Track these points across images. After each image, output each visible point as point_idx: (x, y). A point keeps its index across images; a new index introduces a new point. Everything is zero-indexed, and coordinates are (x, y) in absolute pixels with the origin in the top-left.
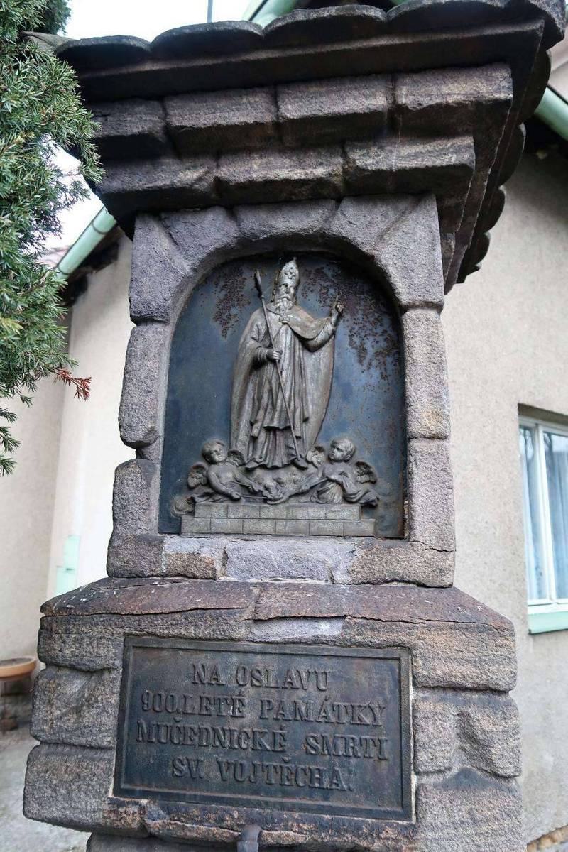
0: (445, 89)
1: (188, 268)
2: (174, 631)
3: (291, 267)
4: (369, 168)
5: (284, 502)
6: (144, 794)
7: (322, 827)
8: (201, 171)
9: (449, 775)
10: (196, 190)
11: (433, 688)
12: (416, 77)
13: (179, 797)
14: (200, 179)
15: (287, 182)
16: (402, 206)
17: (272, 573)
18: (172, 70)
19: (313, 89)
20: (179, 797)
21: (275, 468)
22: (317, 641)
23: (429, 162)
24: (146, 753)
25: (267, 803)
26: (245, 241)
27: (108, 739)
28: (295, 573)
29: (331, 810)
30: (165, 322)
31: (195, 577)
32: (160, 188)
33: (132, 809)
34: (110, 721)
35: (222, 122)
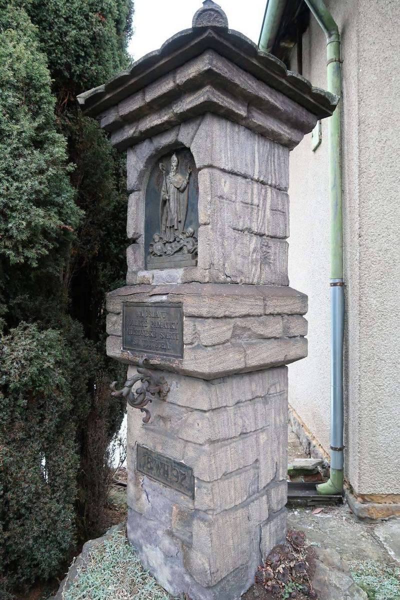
0: (189, 72)
1: (142, 167)
2: (131, 300)
3: (174, 158)
4: (178, 112)
5: (172, 255)
6: (129, 349)
7: (162, 360)
8: (134, 129)
9: (194, 345)
10: (135, 136)
11: (189, 317)
12: (182, 69)
13: (135, 350)
14: (134, 132)
15: (157, 126)
16: (198, 122)
17: (164, 281)
18: (113, 96)
19: (192, 63)
20: (135, 350)
21: (171, 242)
22: (162, 302)
23: (198, 102)
24: (129, 338)
25: (156, 353)
26: (157, 151)
27: (120, 334)
28: (169, 281)
29: (167, 355)
30: (139, 190)
31: (145, 284)
32: (125, 139)
33: (125, 353)
34: (120, 328)
35: (131, 110)
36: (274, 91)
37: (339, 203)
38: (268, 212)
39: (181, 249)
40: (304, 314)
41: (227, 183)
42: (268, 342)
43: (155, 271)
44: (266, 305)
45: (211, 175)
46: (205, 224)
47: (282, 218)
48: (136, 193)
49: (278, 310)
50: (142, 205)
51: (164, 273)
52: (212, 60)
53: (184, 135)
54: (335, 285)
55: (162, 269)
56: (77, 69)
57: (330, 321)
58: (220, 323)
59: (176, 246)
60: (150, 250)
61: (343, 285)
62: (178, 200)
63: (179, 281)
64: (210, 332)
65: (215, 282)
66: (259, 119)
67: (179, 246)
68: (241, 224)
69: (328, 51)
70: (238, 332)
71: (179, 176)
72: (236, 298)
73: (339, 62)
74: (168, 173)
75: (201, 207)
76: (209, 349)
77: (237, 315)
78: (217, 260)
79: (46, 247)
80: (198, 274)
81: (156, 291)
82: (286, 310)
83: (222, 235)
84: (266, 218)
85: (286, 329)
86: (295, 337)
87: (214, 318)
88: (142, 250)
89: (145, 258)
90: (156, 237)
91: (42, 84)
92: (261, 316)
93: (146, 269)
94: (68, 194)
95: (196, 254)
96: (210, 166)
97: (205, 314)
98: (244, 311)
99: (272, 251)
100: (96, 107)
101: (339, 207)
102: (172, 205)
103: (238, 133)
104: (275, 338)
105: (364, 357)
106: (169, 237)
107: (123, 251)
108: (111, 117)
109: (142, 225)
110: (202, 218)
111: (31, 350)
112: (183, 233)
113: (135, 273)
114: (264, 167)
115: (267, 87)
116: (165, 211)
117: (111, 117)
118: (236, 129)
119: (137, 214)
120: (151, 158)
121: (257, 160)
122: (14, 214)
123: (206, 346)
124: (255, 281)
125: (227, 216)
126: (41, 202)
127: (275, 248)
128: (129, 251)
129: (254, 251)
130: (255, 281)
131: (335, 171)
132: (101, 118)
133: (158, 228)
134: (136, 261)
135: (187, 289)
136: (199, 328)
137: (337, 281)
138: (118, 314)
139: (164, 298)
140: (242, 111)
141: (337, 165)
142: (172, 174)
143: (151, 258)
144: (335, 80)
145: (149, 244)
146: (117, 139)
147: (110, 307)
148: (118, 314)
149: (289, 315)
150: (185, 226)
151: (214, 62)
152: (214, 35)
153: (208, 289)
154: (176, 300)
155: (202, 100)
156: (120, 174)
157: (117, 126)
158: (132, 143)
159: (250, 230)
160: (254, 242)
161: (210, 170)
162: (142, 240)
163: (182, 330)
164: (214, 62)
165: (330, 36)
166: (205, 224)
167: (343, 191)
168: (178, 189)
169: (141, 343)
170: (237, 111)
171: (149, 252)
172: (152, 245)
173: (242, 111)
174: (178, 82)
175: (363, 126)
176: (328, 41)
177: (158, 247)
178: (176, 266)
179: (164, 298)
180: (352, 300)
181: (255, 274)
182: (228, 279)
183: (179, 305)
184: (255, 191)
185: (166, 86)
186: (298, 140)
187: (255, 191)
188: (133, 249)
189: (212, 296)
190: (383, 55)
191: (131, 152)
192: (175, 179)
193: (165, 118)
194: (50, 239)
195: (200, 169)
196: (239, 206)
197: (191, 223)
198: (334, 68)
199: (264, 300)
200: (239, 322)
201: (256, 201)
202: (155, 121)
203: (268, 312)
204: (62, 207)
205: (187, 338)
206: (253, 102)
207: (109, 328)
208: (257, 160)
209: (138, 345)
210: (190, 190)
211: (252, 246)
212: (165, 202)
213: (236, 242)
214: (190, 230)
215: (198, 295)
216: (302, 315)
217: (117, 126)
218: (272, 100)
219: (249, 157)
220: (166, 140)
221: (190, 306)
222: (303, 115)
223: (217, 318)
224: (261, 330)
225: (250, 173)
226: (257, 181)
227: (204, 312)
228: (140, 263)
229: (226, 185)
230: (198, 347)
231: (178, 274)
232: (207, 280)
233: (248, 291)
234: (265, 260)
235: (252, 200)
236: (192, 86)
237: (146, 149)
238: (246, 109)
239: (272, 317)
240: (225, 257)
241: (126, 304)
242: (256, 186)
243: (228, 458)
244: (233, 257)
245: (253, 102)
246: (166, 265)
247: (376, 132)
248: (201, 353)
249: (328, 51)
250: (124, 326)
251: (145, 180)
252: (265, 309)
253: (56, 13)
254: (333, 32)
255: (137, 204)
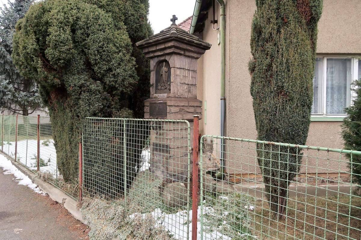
3: (164, 63)
27: (149, 112)
30: (154, 71)
36: (191, 46)
37: (224, 69)
38: (190, 78)
39: (166, 88)
40: (201, 107)
41: (179, 71)
42: (190, 113)
43: (159, 94)
44: (189, 103)
45: (174, 70)
46: (173, 82)
47: (195, 79)
48: (153, 72)
49: (192, 105)
50: (155, 75)
51: (161, 95)
52: (174, 43)
53: (167, 58)
54: (222, 99)
55: (161, 93)
56: (135, 35)
57: (220, 113)
58: (176, 107)
59: (165, 87)
60: (157, 88)
61: (225, 99)
62: (165, 75)
63: (166, 97)
64: (173, 109)
65: (175, 97)
66: (187, 54)
67: (166, 87)
68: (182, 82)
69: (221, 11)
70: (181, 110)
71: (166, 68)
72: (181, 101)
73: (224, 15)
74: (162, 67)
75: (171, 78)
76: (173, 113)
77: (181, 105)
78: (176, 91)
79: (131, 88)
80: (171, 95)
81: (159, 99)
82: (195, 105)
83: (177, 85)
84: (190, 80)
85: (195, 110)
86: (198, 113)
87: (175, 106)
88: (155, 88)
89: (156, 90)
90: (159, 85)
91: (100, 5)
92: (188, 106)
93: (156, 93)
94: (135, 75)
95: (170, 90)
96: (174, 67)
97: (172, 105)
98: (183, 104)
99: (191, 89)
100: (142, 47)
101: (223, 70)
102: (164, 76)
103: (182, 58)
104: (192, 113)
105: (230, 125)
106: (163, 84)
107: (149, 88)
108: (146, 50)
109: (155, 81)
110: (172, 81)
111: (127, 115)
112: (167, 84)
113: (153, 95)
114: (189, 66)
115: (189, 46)
116: (162, 77)
117: (146, 50)
118: (181, 56)
119: (153, 77)
120: (157, 63)
121: (187, 64)
122: (126, 80)
123: (173, 113)
124: (186, 97)
125: (178, 80)
126: (131, 76)
127: (192, 88)
128: (151, 89)
129: (186, 89)
130: (186, 97)
131: (222, 57)
132: (143, 50)
133: (159, 82)
134: (153, 91)
135: (168, 99)
136: (171, 108)
137: (223, 98)
138: (148, 106)
139: (162, 101)
140: (182, 53)
141: (223, 55)
142: (163, 67)
143: (157, 90)
144: (223, 22)
145: (157, 86)
146: (147, 56)
147: (146, 104)
148: (148, 106)
149: (196, 107)
150: (167, 82)
151: (175, 43)
152: (175, 38)
153: (173, 99)
154: (165, 102)
155: (172, 51)
156: (148, 66)
157: (149, 53)
158: (152, 58)
159: (185, 83)
160: (186, 87)
161: (174, 68)
162: (155, 85)
163: (167, 109)
164: (175, 43)
165: (221, 5)
166: (173, 82)
167: (225, 64)
168: (165, 72)
169: (155, 114)
170: (181, 53)
171: (157, 89)
172: (158, 87)
173: (182, 53)
174: (166, 46)
175: (230, 42)
176: (221, 7)
177: (160, 87)
178: (165, 93)
179: (162, 101)
180: (227, 104)
181: (186, 95)
182: (179, 96)
183: (166, 103)
184: (187, 73)
185: (163, 46)
186: (200, 57)
187: (187, 73)
188: (152, 88)
189: (175, 100)
190: (238, 16)
191: (152, 60)
192: (164, 69)
193: (162, 53)
194: (132, 86)
195: (171, 68)
196: (182, 77)
197: (169, 81)
198: (222, 17)
199: (188, 102)
200: (182, 108)
201: (187, 75)
202: (159, 53)
203: (189, 105)
204: (134, 77)
205: (168, 111)
206: (185, 50)
207: (145, 110)
208: (187, 64)
209: (154, 115)
210: (169, 73)
211: (185, 88)
212: (162, 75)
213: (181, 86)
214: (169, 83)
215: (171, 100)
216: (200, 107)
217: (149, 53)
218: (190, 49)
219: (185, 64)
220: (162, 58)
221: (169, 103)
222: (200, 50)
223: (176, 106)
224: (187, 110)
225: (185, 68)
226: (187, 70)
227: (172, 104)
228: (154, 91)
229: (178, 72)
230: (171, 113)
231: (166, 95)
232: (173, 96)
233: (184, 100)
234: (189, 91)
235: (186, 75)
236: (170, 47)
237: (156, 60)
238: (183, 52)
239: (191, 107)
240: (178, 91)
241: (151, 103)
242: (187, 71)
243: (178, 143)
244: (180, 90)
245: (185, 50)
246: (162, 92)
247: (235, 44)
248: (171, 115)
249: (221, 11)
250: (150, 109)
251: (156, 68)
252: (189, 105)
253: (130, 21)
254: (222, 4)
255: (153, 75)
